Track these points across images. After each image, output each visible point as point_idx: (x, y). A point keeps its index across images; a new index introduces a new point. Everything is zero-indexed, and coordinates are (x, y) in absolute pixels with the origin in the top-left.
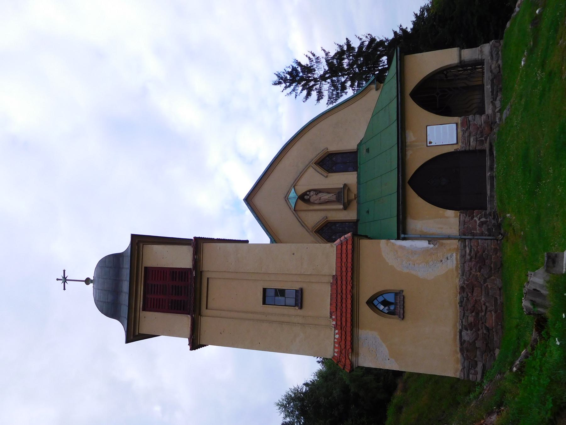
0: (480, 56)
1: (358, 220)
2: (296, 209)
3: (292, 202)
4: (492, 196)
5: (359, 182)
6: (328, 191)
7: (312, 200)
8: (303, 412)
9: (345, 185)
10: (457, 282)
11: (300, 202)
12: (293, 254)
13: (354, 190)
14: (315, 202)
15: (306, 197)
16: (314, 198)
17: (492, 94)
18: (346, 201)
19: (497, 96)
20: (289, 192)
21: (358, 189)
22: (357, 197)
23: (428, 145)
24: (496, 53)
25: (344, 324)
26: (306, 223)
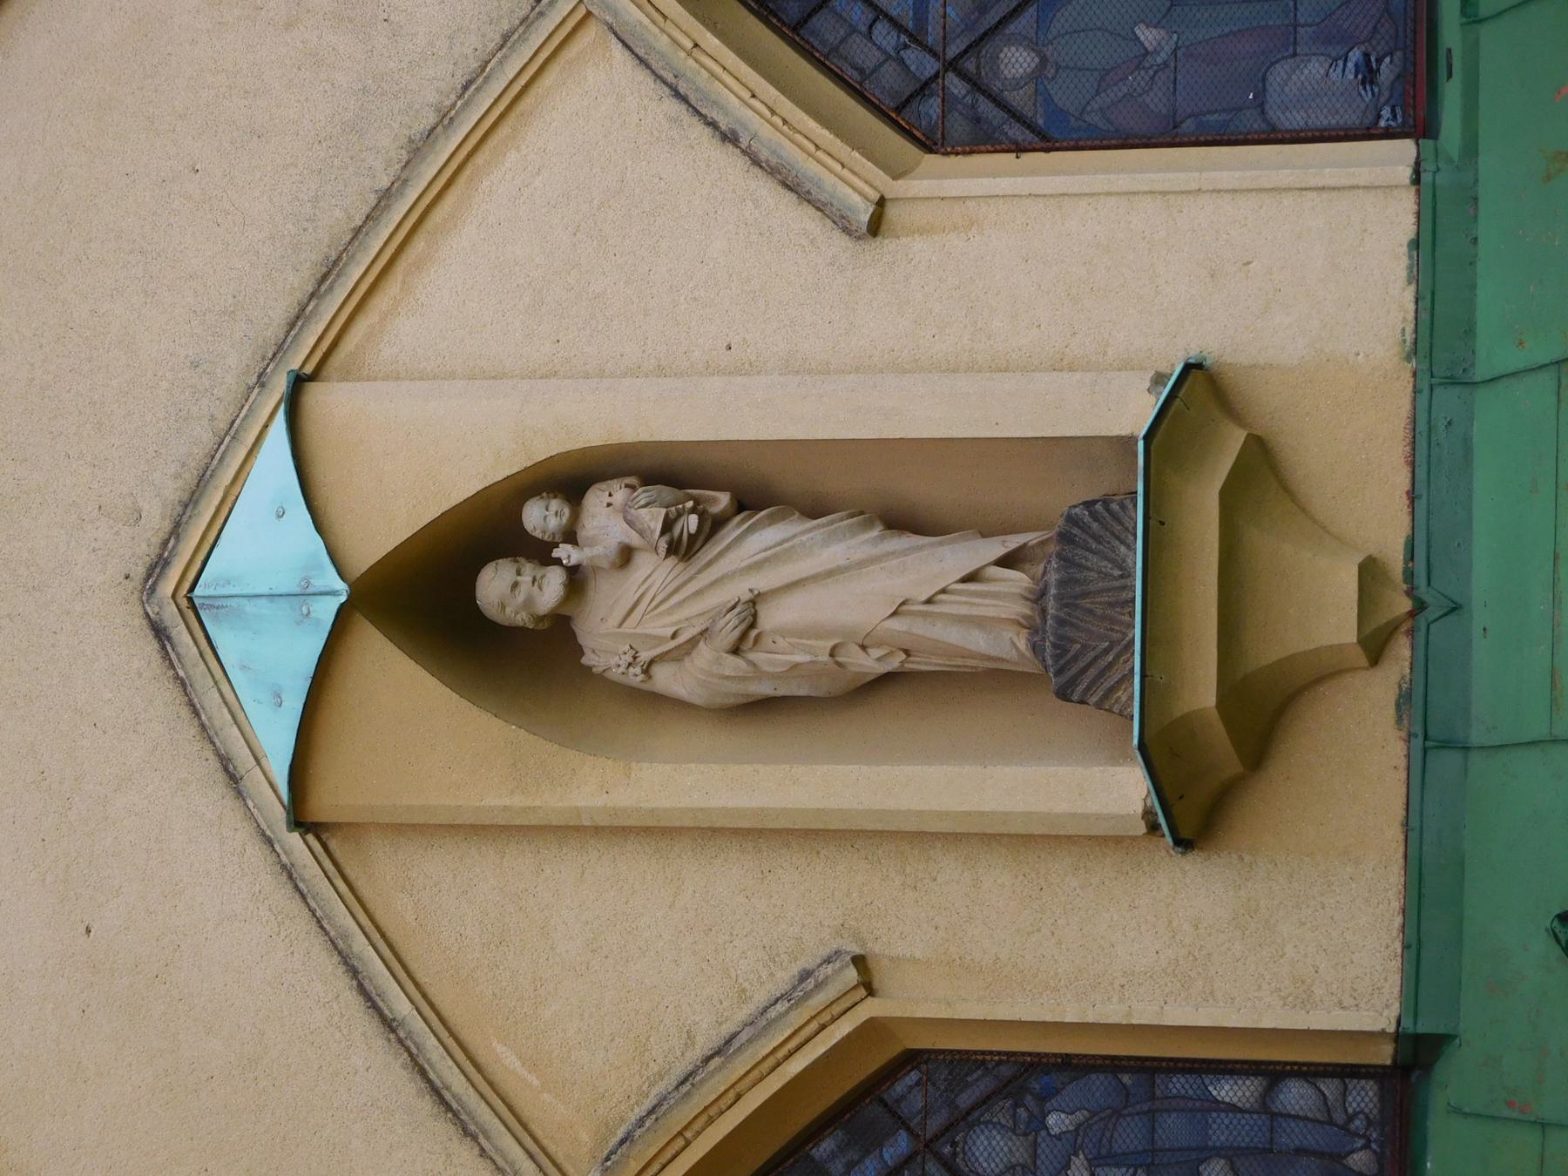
1: (1415, 1057)
2: (326, 802)
3: (268, 663)
5: (1441, 351)
6: (893, 496)
7: (611, 632)
9: (1196, 393)
11: (388, 671)
13: (1359, 481)
14: (667, 679)
15: (504, 590)
16: (640, 609)
18: (1200, 689)
20: (203, 499)
21: (1437, 462)
22: (1416, 609)
26: (504, 1059)
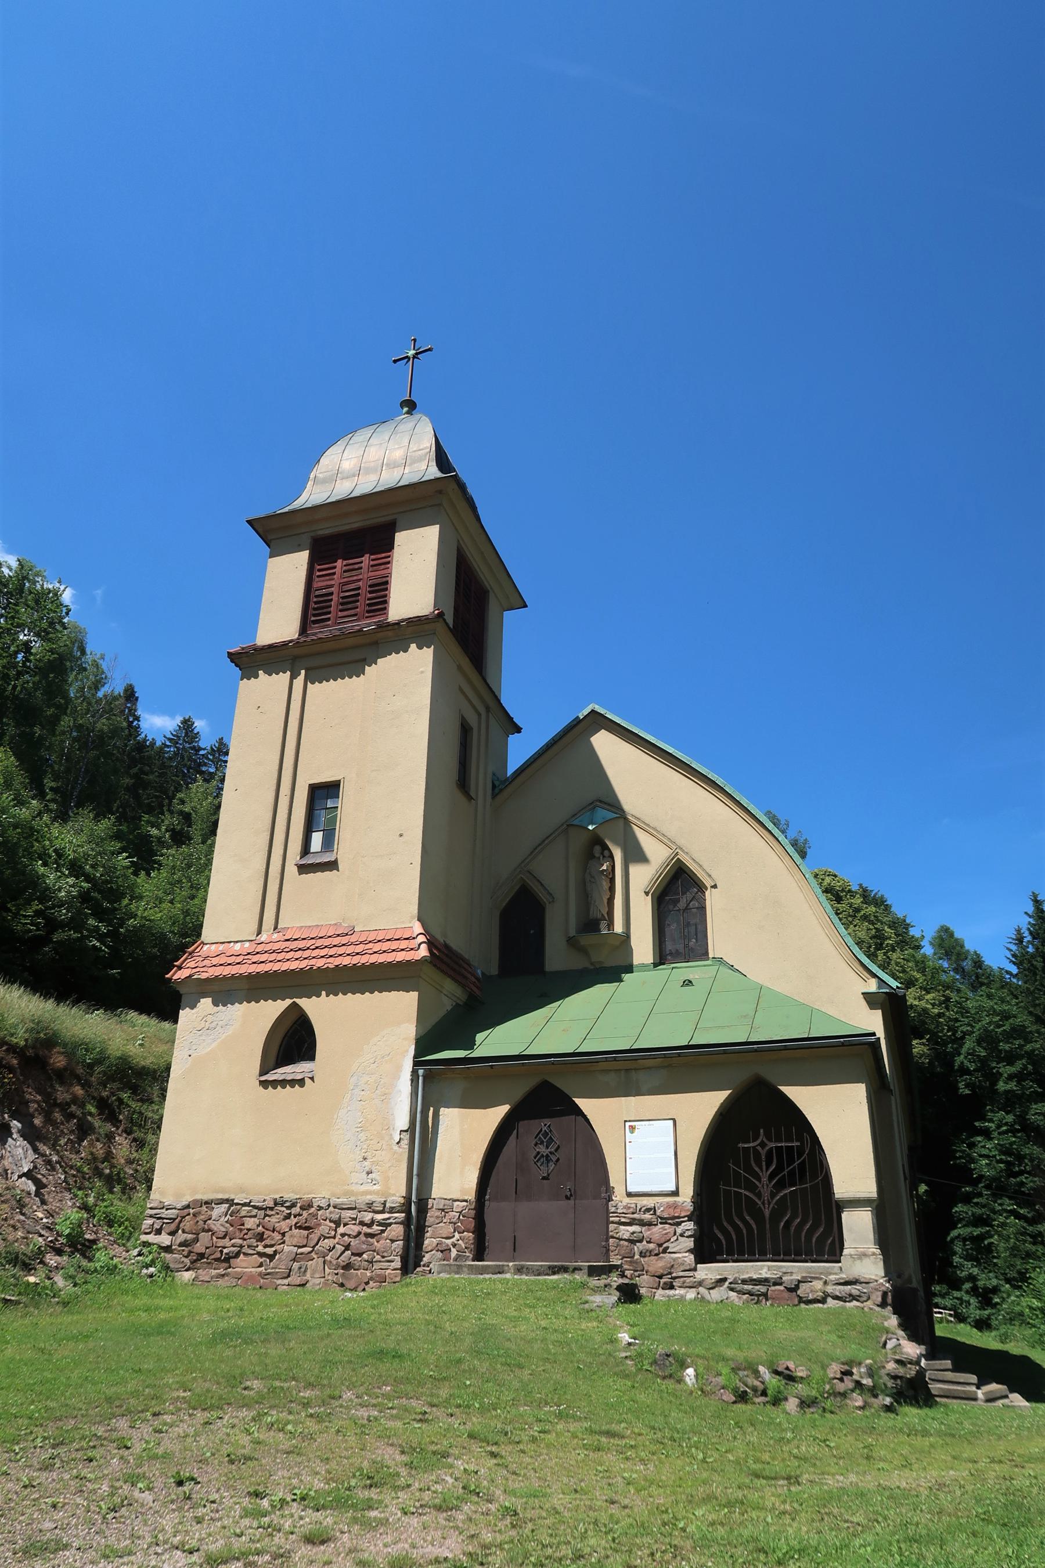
0: (852, 1251)
4: (529, 1271)
8: (10, 849)
10: (321, 1195)
12: (401, 835)
17: (744, 1282)
19: (741, 1292)
23: (628, 1124)
24: (855, 1292)
25: (255, 958)
